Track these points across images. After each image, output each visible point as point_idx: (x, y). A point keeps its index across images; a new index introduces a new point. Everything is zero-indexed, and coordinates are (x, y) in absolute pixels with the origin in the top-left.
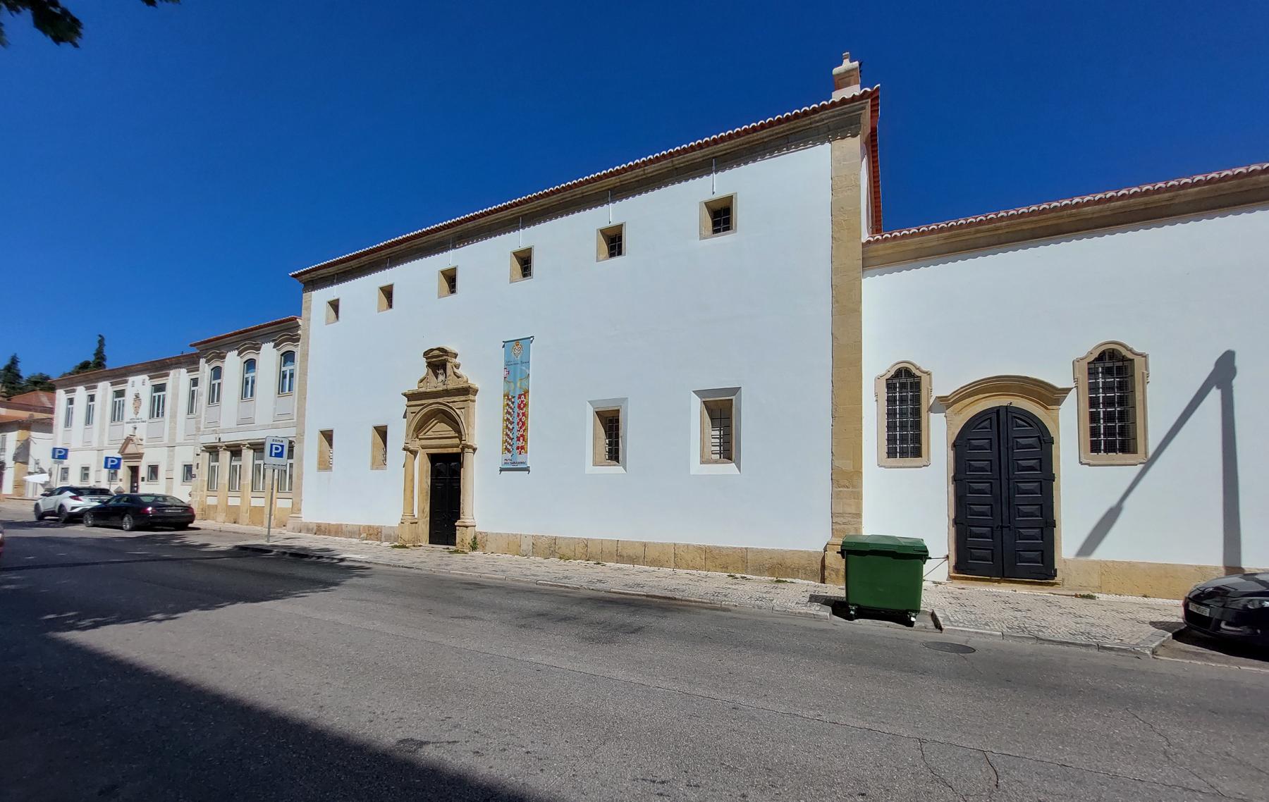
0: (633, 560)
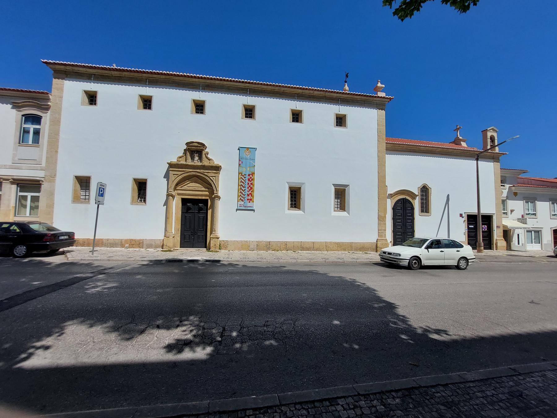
0: (308, 249)
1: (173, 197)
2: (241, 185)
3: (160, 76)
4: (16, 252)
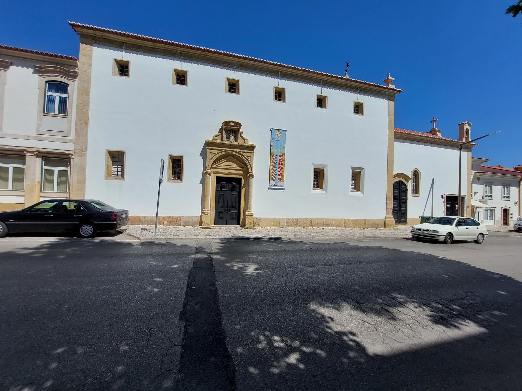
0: (329, 226)
1: (210, 174)
2: (273, 165)
3: (196, 52)
4: (82, 231)
